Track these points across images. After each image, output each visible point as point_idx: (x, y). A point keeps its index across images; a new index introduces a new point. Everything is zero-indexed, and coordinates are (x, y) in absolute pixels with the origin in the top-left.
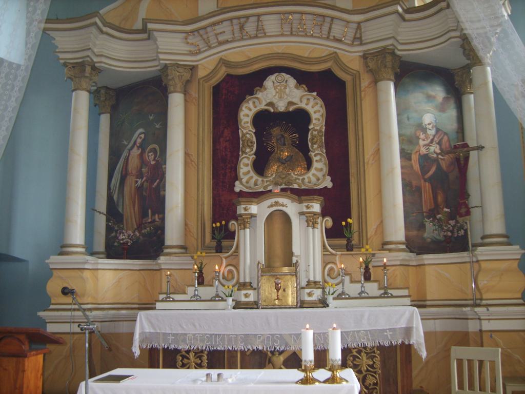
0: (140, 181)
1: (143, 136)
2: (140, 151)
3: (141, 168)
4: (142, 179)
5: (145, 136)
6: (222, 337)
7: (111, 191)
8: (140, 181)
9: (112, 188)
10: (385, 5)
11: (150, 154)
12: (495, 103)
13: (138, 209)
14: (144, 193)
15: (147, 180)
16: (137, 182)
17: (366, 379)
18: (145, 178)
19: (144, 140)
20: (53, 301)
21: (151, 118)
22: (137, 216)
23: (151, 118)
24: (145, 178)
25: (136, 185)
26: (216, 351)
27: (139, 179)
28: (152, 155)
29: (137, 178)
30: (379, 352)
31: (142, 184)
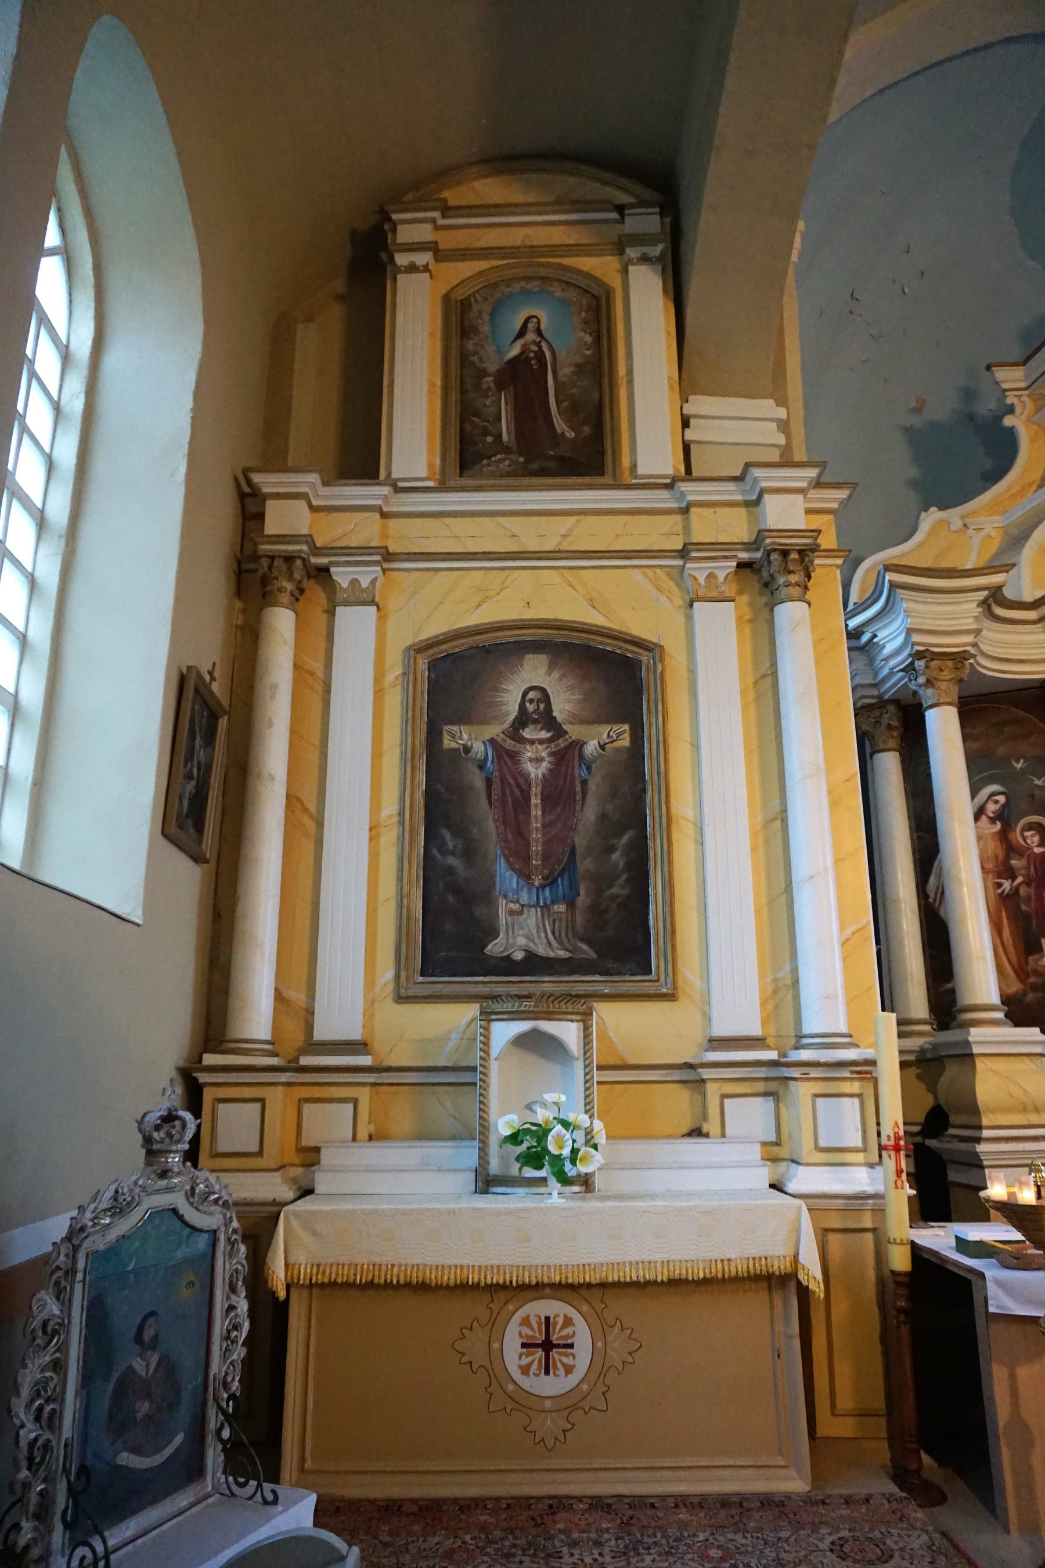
0: (1007, 885)
1: (1002, 799)
2: (999, 825)
3: (1007, 858)
4: (1013, 880)
5: (1007, 798)
6: (594, 1267)
7: (931, 900)
8: (1007, 885)
9: (932, 895)
10: (539, 555)
11: (1028, 834)
12: (534, 1178)
13: (1011, 932)
14: (1024, 907)
15: (1027, 883)
16: (1000, 885)
17: (537, 1284)
18: (1020, 879)
19: (1004, 806)
20: (985, 1122)
21: (1019, 766)
22: (1011, 950)
23: (1019, 766)
24: (1020, 879)
25: (1000, 891)
26: (940, 1504)
27: (1007, 879)
28: (1032, 836)
29: (999, 878)
30: (386, 227)
31: (1016, 891)
